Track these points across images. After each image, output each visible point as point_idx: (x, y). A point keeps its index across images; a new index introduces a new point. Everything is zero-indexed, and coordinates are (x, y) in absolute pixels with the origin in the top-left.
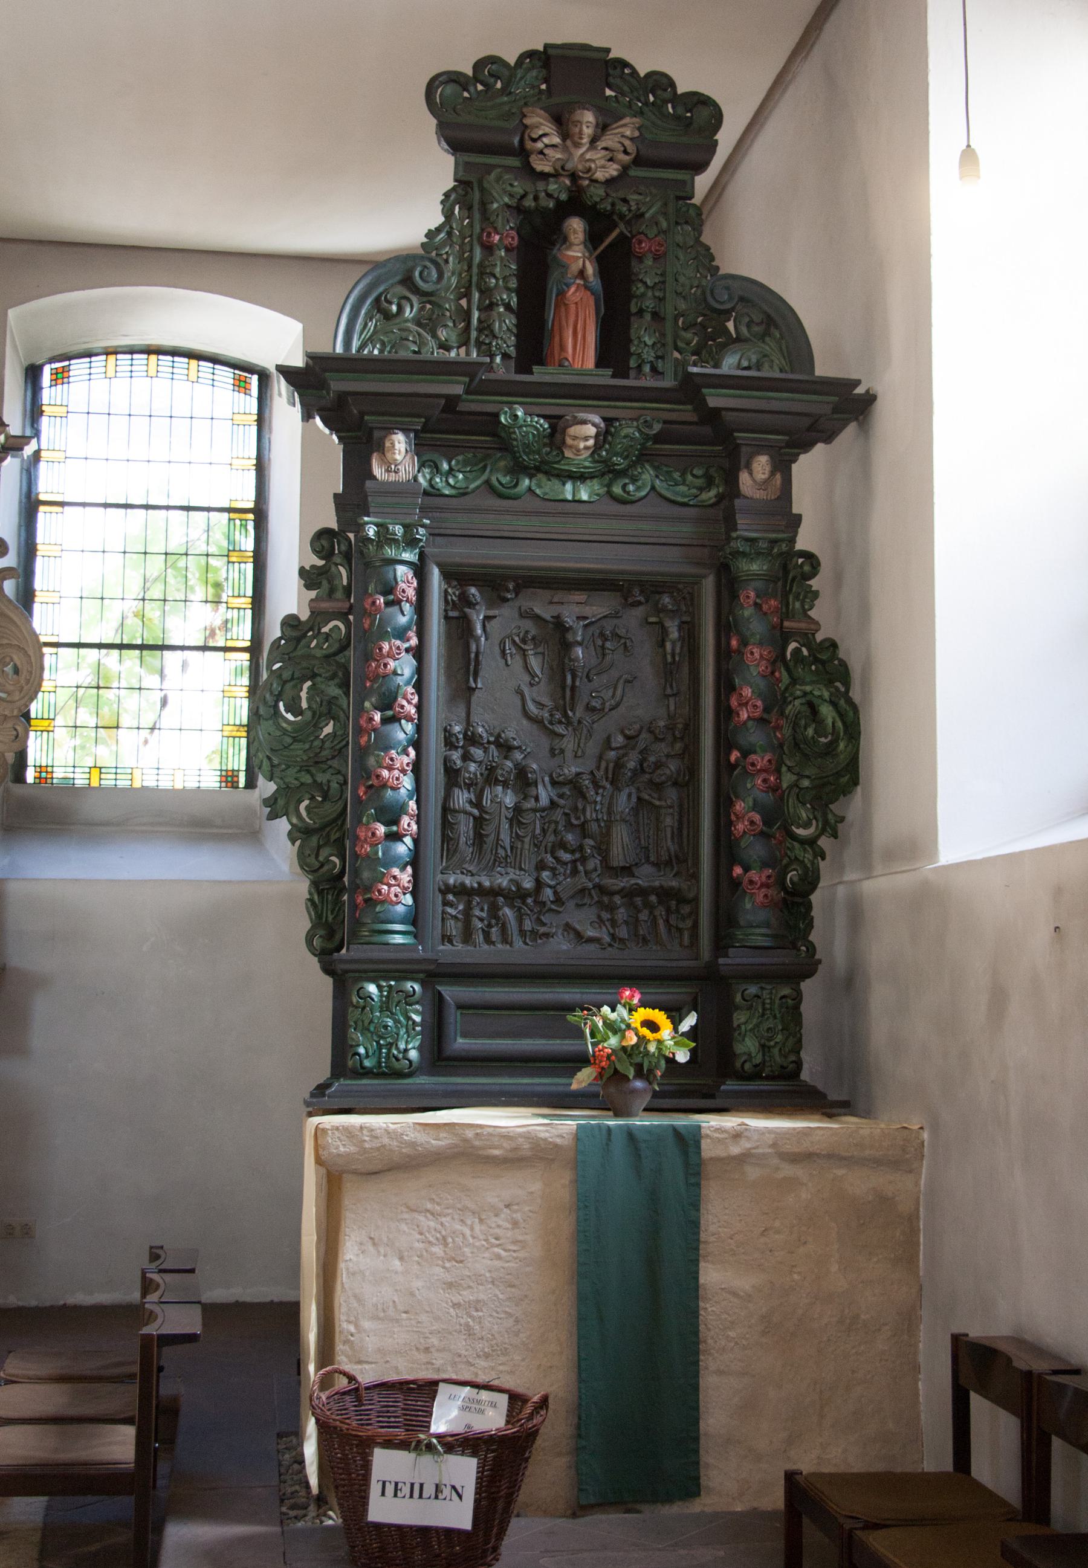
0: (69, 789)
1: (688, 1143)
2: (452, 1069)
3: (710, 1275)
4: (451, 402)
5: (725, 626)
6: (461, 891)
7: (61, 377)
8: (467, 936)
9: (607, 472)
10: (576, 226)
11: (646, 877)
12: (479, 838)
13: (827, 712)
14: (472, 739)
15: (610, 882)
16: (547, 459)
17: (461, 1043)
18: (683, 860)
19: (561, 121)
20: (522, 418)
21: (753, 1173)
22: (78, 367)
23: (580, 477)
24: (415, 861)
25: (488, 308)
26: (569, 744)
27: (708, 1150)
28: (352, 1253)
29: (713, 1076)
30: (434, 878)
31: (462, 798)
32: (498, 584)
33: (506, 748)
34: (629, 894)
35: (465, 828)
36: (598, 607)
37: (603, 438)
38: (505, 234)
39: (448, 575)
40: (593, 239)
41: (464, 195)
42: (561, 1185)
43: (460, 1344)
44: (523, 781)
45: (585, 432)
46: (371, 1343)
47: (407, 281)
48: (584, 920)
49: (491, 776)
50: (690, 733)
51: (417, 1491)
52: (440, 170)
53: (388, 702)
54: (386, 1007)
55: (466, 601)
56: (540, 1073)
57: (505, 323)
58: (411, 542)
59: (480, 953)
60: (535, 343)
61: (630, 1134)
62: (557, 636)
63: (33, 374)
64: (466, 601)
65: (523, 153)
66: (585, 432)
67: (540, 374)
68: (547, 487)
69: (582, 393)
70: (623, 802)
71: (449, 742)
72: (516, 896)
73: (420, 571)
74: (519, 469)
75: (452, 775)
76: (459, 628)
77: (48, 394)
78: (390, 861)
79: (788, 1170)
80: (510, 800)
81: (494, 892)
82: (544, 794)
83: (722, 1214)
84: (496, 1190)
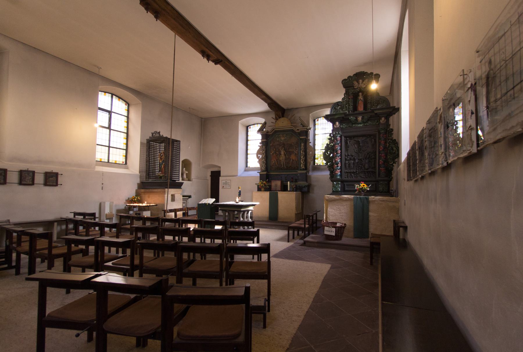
0: (320, 165)
1: (367, 199)
2: (345, 191)
3: (370, 214)
4: (343, 117)
5: (379, 139)
6: (347, 172)
7: (318, 120)
8: (348, 177)
9: (363, 122)
10: (360, 94)
11: (370, 170)
12: (349, 166)
13: (395, 148)
14: (348, 155)
15: (365, 171)
16: (356, 122)
17: (346, 189)
18: (375, 167)
19: (358, 82)
20: (352, 118)
21: (376, 202)
22: (319, 119)
23: (360, 124)
24: (341, 168)
25: (349, 106)
26: (360, 155)
27: (370, 200)
28: (329, 209)
29: (374, 191)
30: (343, 171)
31: (347, 162)
32: (351, 137)
33: (352, 156)
34: (367, 172)
35: (347, 165)
36: (364, 138)
37: (362, 119)
38: (351, 97)
39: (345, 137)
40: (362, 95)
41: (347, 93)
42: (352, 203)
43: (341, 219)
44: (354, 160)
45: (360, 118)
46: (331, 218)
47: (338, 105)
48: (362, 175)
49: (350, 159)
50: (375, 152)
51: (329, 231)
52: (344, 91)
53: (337, 152)
54: (336, 184)
55: (347, 140)
56: (352, 192)
57: (351, 107)
58: (339, 134)
59: (349, 179)
60: (355, 108)
61: (360, 198)
62: (358, 143)
63: (314, 121)
64: (347, 140)
65: (353, 86)
66: (360, 118)
67: (356, 112)
68: (357, 125)
69: (360, 114)
70: (367, 161)
71: (346, 156)
72: (353, 173)
73: (341, 137)
74: (353, 124)
75: (346, 159)
76: (346, 143)
77: (316, 122)
78: (337, 169)
79: (381, 202)
80: (353, 162)
81: (351, 172)
82: (357, 161)
83: (372, 207)
84: (345, 203)
